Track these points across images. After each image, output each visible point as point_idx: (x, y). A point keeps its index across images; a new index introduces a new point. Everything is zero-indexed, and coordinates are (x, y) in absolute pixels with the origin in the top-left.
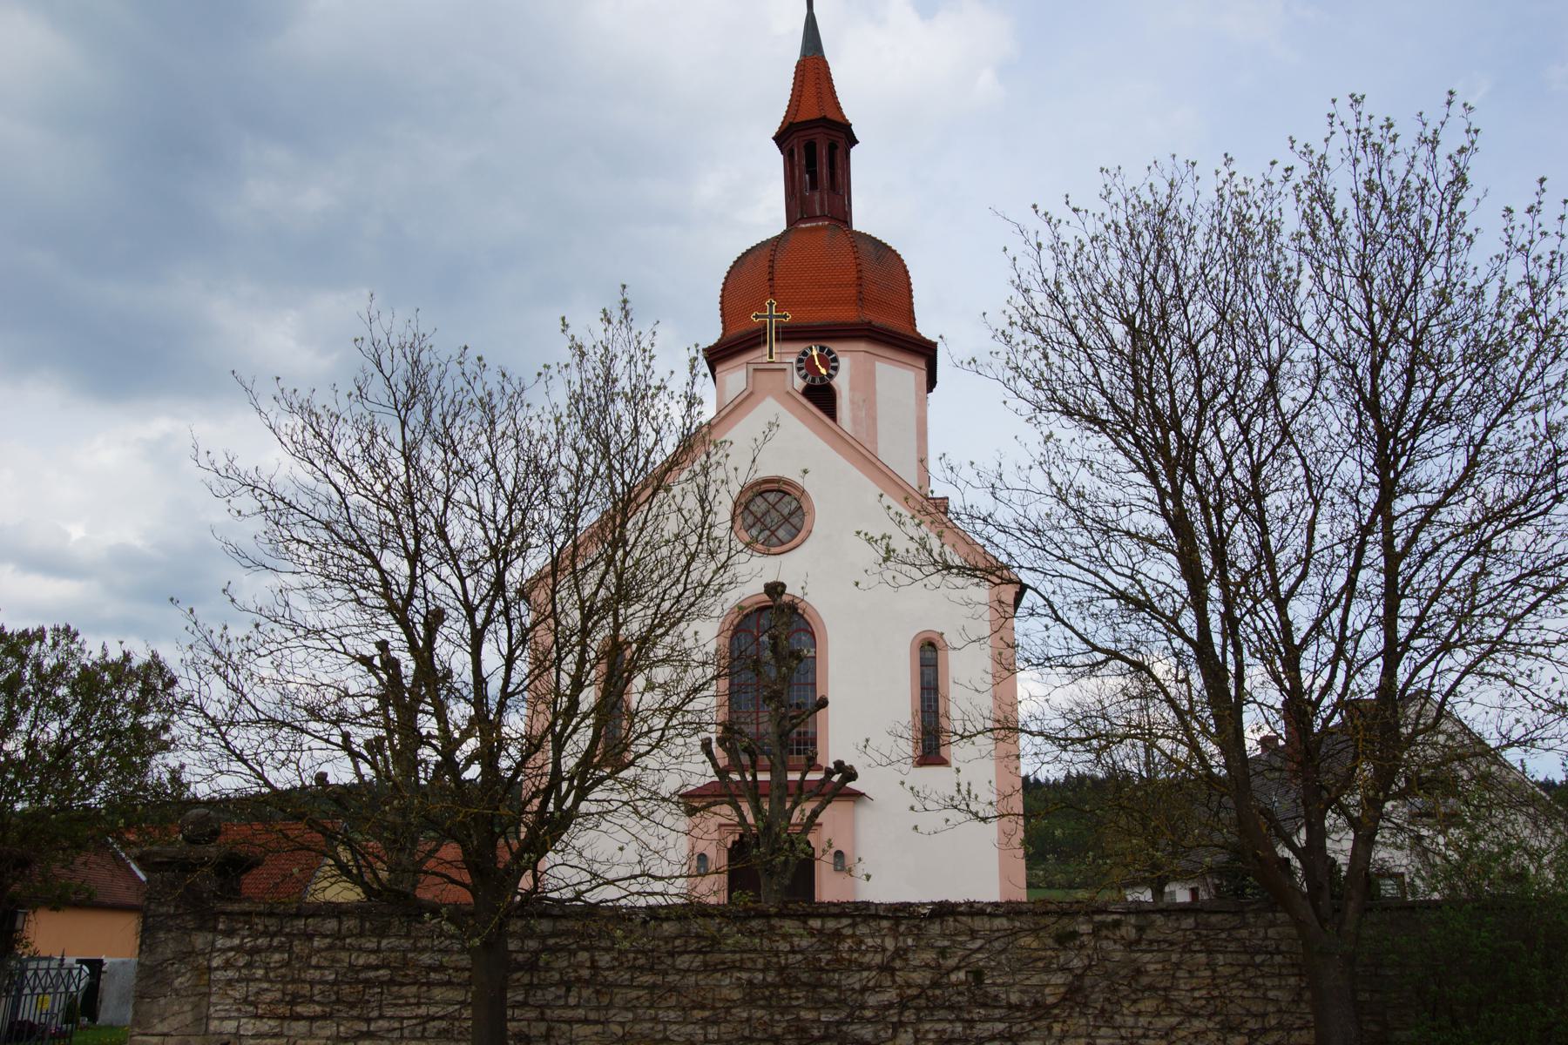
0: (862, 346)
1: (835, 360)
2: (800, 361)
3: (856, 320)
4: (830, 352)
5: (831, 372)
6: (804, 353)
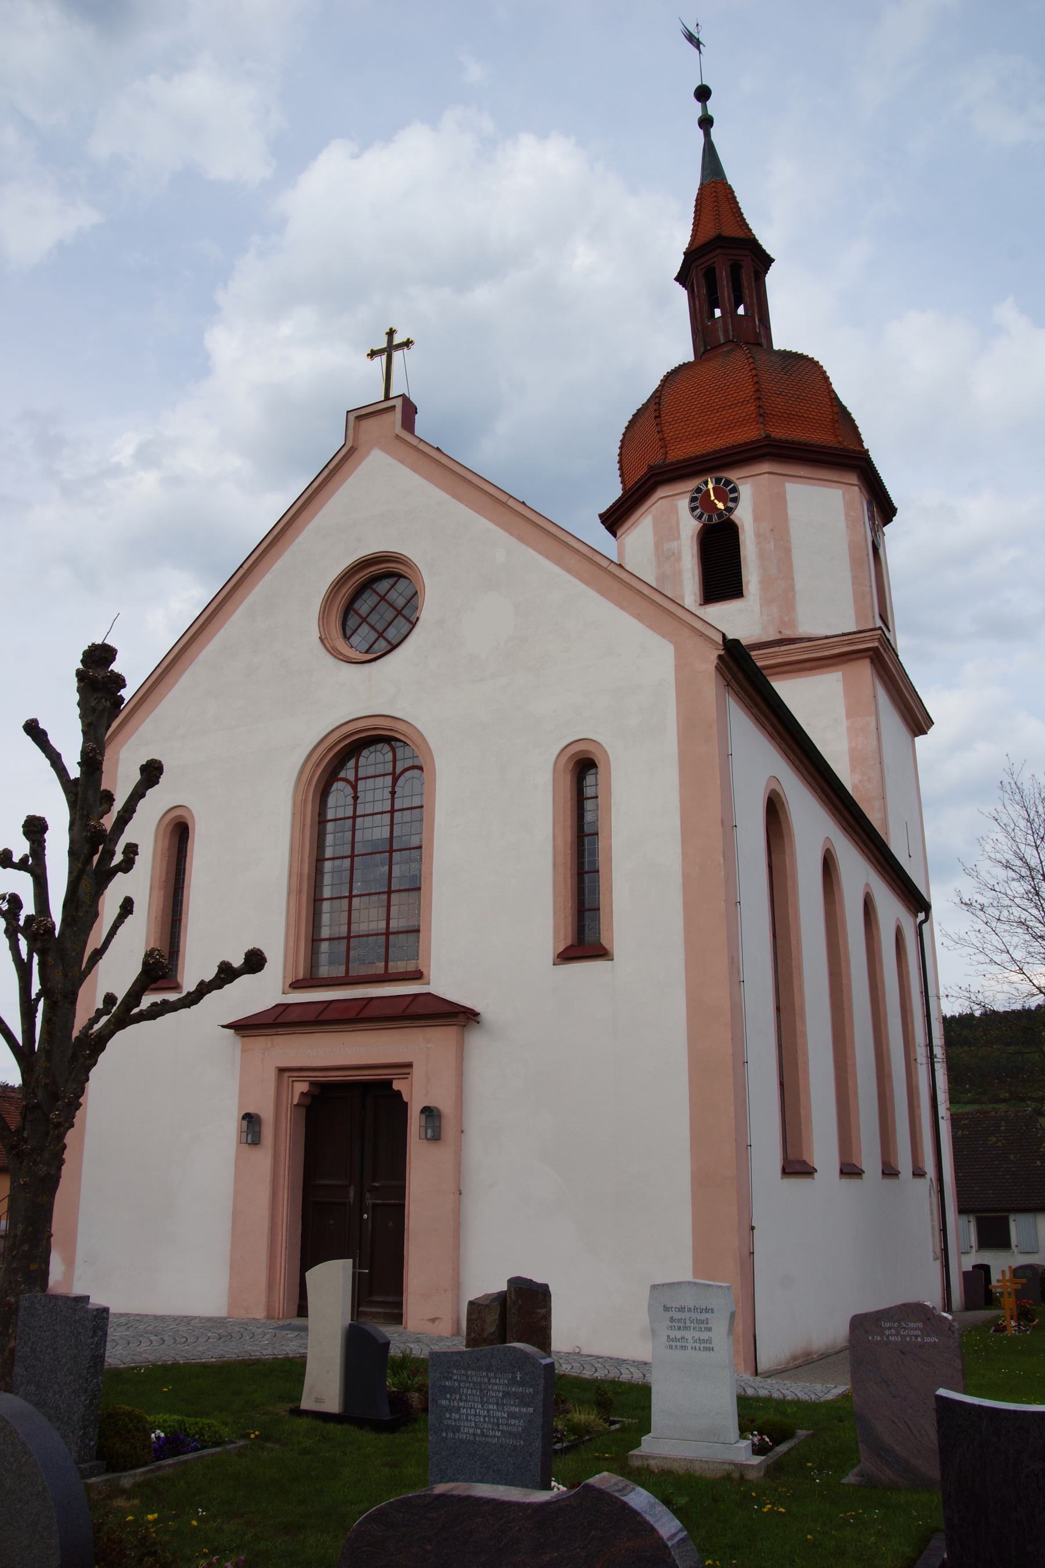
0: (765, 467)
1: (735, 490)
2: (693, 500)
4: (728, 482)
5: (731, 504)
6: (698, 490)
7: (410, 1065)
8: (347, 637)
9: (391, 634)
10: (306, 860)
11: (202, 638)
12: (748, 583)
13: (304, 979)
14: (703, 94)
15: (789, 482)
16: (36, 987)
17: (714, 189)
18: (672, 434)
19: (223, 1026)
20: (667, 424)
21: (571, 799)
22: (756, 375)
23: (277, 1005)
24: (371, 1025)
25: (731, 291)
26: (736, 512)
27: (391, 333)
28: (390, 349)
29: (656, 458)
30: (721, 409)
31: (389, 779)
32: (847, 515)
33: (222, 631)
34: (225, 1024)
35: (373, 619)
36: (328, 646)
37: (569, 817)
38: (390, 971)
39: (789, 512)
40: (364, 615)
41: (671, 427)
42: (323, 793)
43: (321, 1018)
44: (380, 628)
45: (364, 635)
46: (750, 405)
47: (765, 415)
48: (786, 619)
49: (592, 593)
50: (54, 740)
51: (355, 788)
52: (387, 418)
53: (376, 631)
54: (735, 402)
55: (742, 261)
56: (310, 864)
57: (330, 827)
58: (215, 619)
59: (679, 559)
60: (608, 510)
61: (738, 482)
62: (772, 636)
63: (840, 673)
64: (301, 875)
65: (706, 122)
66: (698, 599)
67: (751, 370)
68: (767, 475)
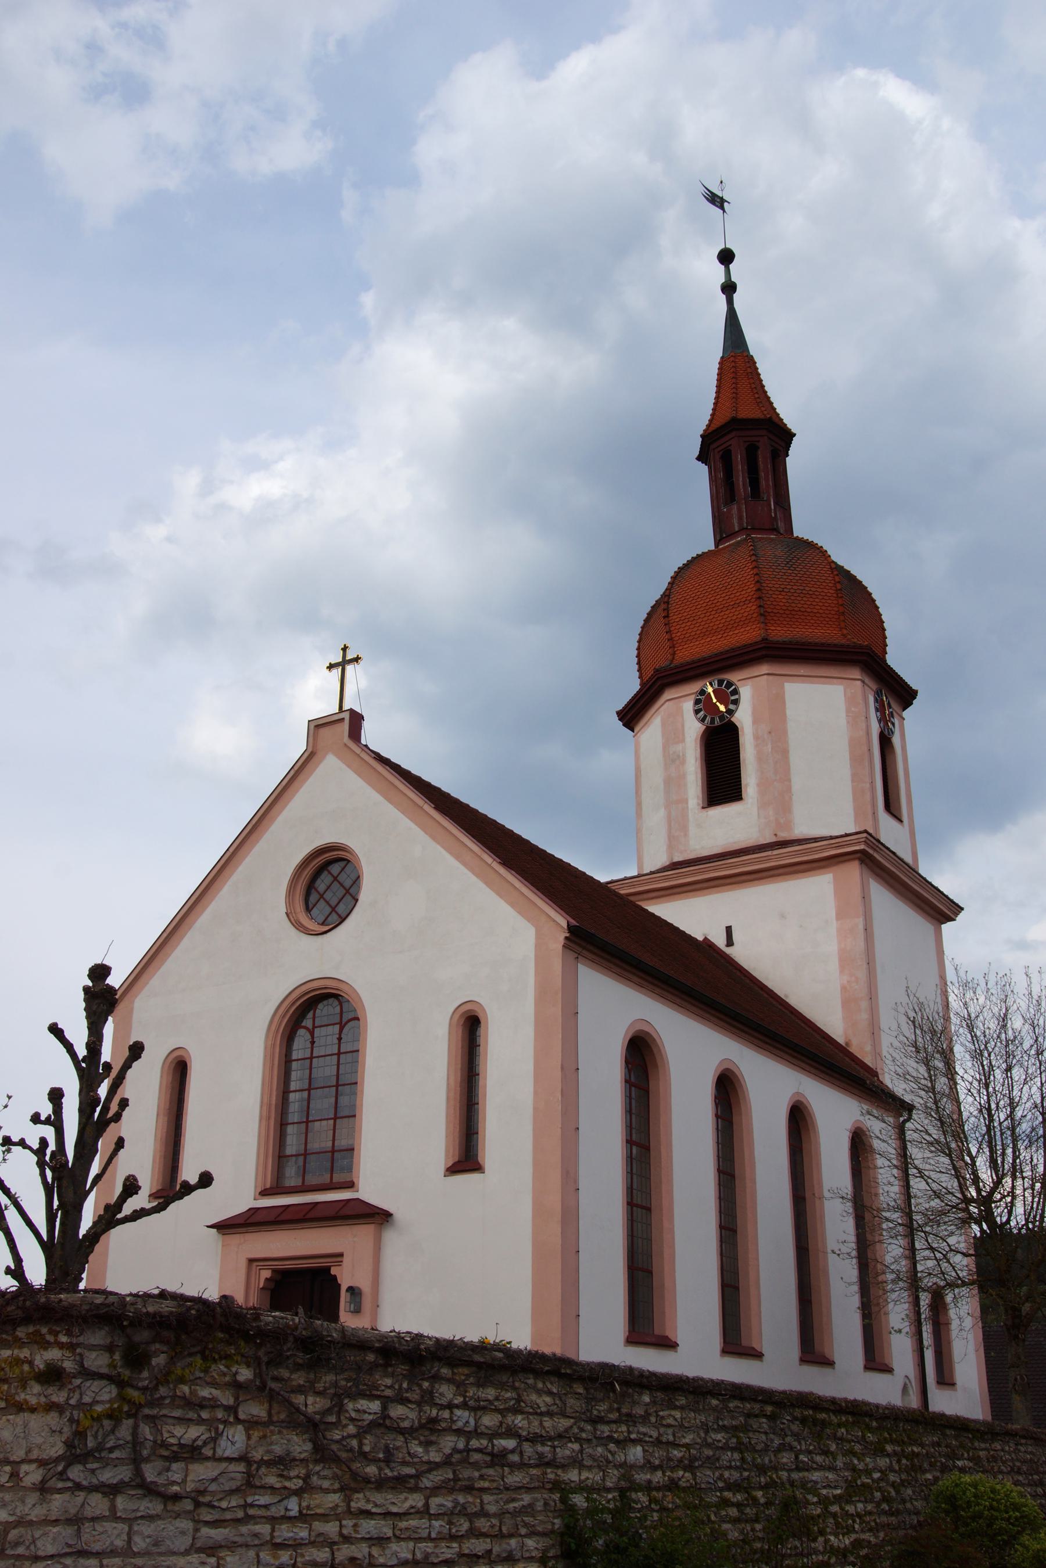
0: (765, 669)
1: (736, 692)
2: (697, 702)
4: (730, 684)
5: (732, 707)
7: (341, 1255)
8: (308, 909)
9: (341, 909)
10: (274, 1093)
11: (198, 908)
12: (747, 785)
13: (271, 1188)
14: (726, 257)
15: (787, 682)
16: (56, 1203)
17: (733, 364)
18: (679, 634)
19: (208, 1227)
20: (675, 624)
21: (462, 1047)
22: (757, 574)
23: (250, 1209)
24: (315, 1224)
25: (747, 475)
26: (737, 715)
27: (345, 649)
28: (343, 664)
29: (662, 662)
30: (725, 609)
31: (337, 1027)
32: (848, 711)
33: (213, 903)
34: (209, 1224)
35: (328, 896)
36: (292, 919)
37: (459, 1062)
38: (334, 1181)
39: (788, 712)
40: (322, 892)
41: (678, 627)
43: (279, 1219)
44: (333, 904)
45: (321, 910)
46: (751, 604)
48: (782, 821)
49: (481, 885)
50: (68, 1035)
51: (312, 1034)
53: (330, 906)
54: (738, 602)
55: (758, 441)
56: (277, 1096)
57: (294, 1065)
58: (209, 892)
59: (683, 762)
60: (624, 708)
61: (738, 684)
62: (769, 839)
64: (270, 1105)
65: (729, 288)
66: (701, 802)
67: (753, 568)
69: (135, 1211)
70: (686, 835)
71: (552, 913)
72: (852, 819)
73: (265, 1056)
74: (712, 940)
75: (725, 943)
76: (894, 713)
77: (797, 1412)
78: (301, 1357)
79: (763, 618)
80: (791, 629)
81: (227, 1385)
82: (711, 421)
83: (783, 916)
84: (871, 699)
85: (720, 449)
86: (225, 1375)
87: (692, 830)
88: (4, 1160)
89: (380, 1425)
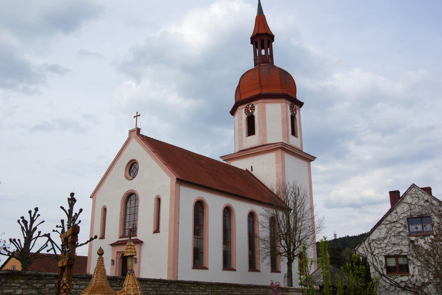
0: (260, 101)
1: (254, 107)
2: (245, 110)
3: (281, 92)
5: (253, 111)
8: (130, 173)
9: (136, 174)
10: (123, 215)
11: (108, 174)
12: (256, 131)
17: (259, 18)
27: (137, 113)
31: (135, 200)
32: (282, 110)
42: (126, 203)
47: (262, 86)
48: (264, 140)
52: (135, 131)
56: (123, 216)
59: (242, 125)
61: (255, 105)
62: (261, 144)
63: (274, 153)
68: (261, 103)
69: (81, 244)
70: (242, 144)
71: (174, 176)
72: (282, 138)
73: (121, 207)
74: (248, 170)
75: (251, 170)
76: (297, 109)
77: (176, 284)
78: (36, 278)
79: (261, 88)
80: (268, 90)
81: (19, 283)
82: (253, 34)
83: (264, 163)
84: (289, 107)
85: (255, 41)
86: (18, 282)
87: (244, 142)
88: (11, 244)
89: (54, 288)
